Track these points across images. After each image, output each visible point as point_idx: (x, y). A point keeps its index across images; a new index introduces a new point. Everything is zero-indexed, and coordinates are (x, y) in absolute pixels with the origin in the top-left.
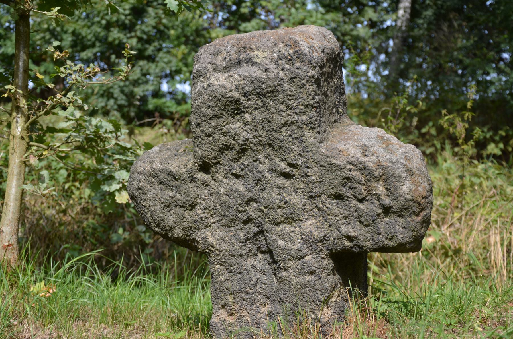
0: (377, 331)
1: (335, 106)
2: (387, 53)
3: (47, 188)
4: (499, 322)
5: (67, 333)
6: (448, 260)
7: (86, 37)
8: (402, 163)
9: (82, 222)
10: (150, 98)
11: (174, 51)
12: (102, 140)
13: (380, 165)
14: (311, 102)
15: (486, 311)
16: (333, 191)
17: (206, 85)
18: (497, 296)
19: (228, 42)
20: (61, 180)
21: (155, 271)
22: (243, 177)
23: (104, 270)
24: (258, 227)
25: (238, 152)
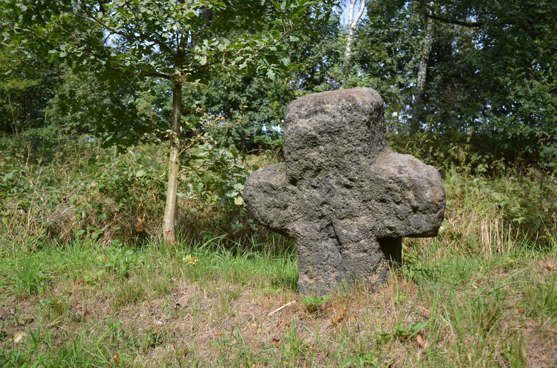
0: (408, 290)
1: (380, 140)
2: (411, 105)
3: (192, 195)
4: (488, 282)
5: (206, 288)
6: (454, 241)
7: (215, 97)
8: (425, 178)
9: (213, 217)
10: (254, 135)
11: (270, 105)
12: (225, 164)
13: (410, 179)
14: (364, 138)
15: (480, 275)
16: (379, 197)
17: (294, 127)
18: (487, 265)
19: (308, 99)
20: (200, 189)
21: (260, 249)
22: (319, 188)
23: (228, 248)
24: (329, 221)
25: (315, 171)
